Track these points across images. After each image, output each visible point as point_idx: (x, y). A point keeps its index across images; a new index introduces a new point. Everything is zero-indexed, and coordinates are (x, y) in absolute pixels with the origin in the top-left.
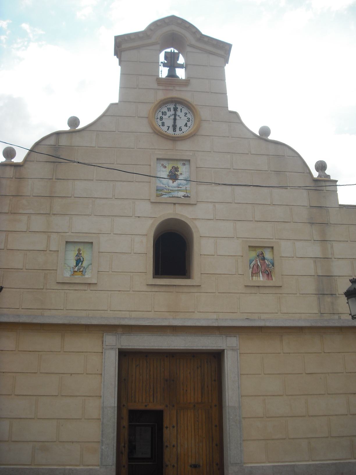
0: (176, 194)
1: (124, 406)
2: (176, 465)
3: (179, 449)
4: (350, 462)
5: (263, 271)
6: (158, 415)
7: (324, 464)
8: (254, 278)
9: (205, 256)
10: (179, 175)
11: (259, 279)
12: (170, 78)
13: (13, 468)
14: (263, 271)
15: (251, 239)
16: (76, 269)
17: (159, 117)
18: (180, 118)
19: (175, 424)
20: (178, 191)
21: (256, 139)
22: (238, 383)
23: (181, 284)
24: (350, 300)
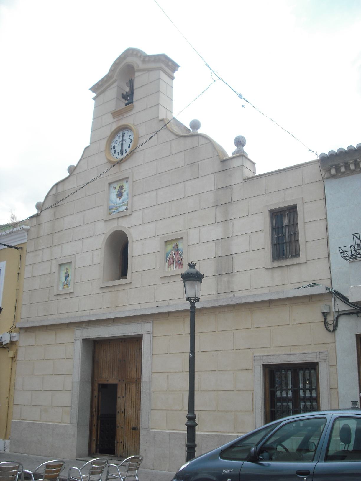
0: (121, 209)
1: (96, 381)
2: (123, 427)
3: (126, 414)
4: (231, 436)
5: (176, 261)
6: (114, 387)
7: (209, 435)
8: (169, 268)
9: (136, 257)
10: (123, 192)
11: (173, 270)
12: (126, 106)
13: (32, 423)
14: (176, 261)
15: (178, 232)
16: (65, 284)
17: (113, 147)
18: (126, 141)
19: (124, 395)
20: (122, 206)
21: (177, 138)
22: (150, 362)
23: (119, 284)
24: (186, 283)
